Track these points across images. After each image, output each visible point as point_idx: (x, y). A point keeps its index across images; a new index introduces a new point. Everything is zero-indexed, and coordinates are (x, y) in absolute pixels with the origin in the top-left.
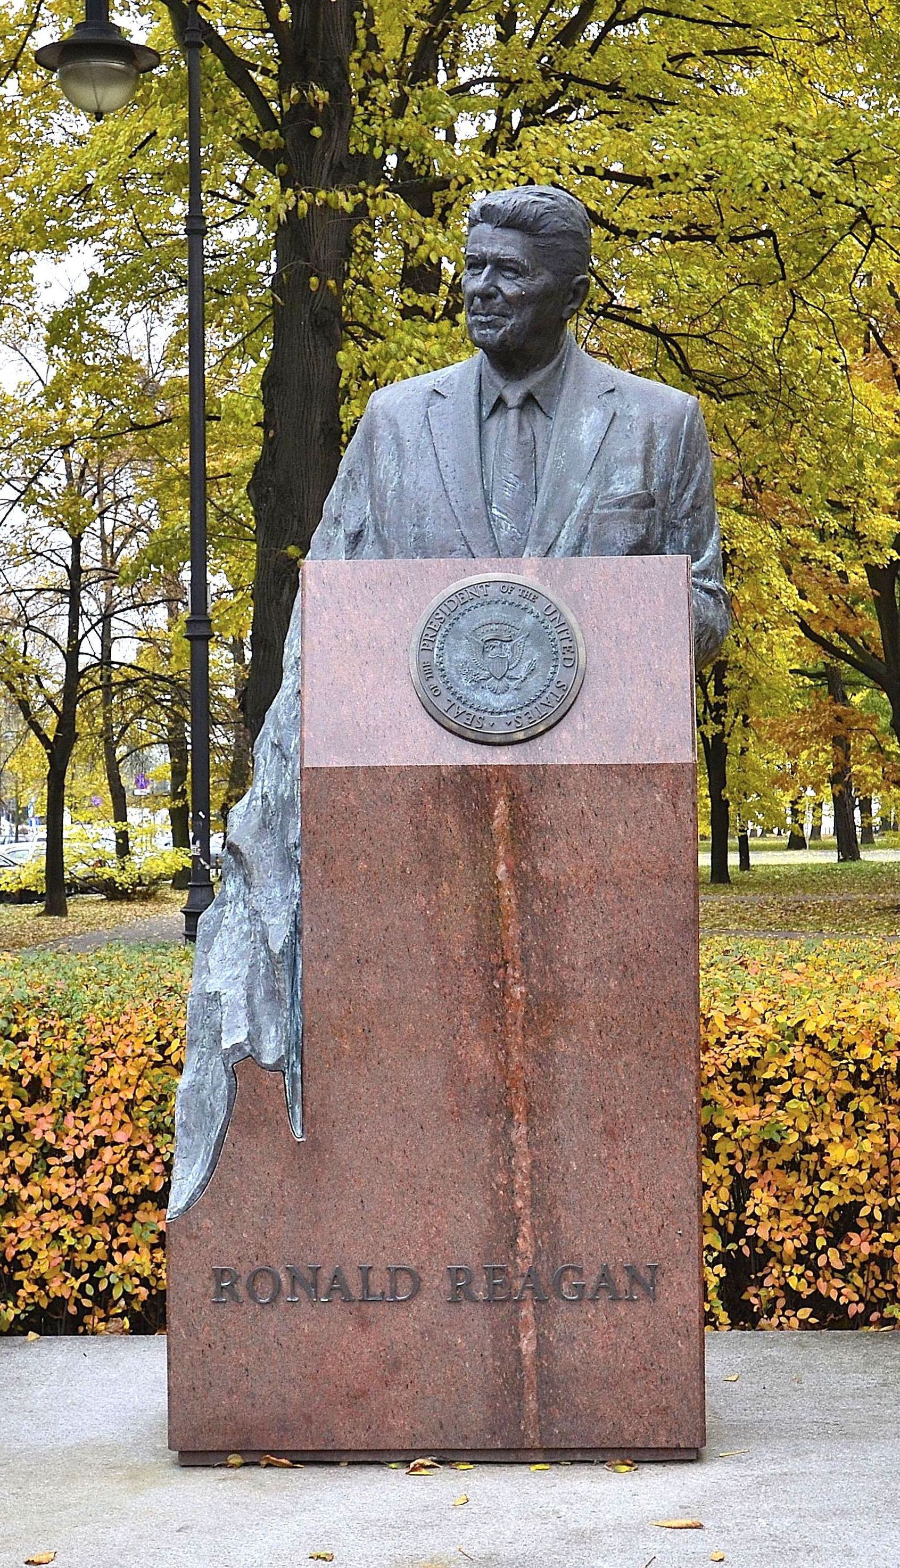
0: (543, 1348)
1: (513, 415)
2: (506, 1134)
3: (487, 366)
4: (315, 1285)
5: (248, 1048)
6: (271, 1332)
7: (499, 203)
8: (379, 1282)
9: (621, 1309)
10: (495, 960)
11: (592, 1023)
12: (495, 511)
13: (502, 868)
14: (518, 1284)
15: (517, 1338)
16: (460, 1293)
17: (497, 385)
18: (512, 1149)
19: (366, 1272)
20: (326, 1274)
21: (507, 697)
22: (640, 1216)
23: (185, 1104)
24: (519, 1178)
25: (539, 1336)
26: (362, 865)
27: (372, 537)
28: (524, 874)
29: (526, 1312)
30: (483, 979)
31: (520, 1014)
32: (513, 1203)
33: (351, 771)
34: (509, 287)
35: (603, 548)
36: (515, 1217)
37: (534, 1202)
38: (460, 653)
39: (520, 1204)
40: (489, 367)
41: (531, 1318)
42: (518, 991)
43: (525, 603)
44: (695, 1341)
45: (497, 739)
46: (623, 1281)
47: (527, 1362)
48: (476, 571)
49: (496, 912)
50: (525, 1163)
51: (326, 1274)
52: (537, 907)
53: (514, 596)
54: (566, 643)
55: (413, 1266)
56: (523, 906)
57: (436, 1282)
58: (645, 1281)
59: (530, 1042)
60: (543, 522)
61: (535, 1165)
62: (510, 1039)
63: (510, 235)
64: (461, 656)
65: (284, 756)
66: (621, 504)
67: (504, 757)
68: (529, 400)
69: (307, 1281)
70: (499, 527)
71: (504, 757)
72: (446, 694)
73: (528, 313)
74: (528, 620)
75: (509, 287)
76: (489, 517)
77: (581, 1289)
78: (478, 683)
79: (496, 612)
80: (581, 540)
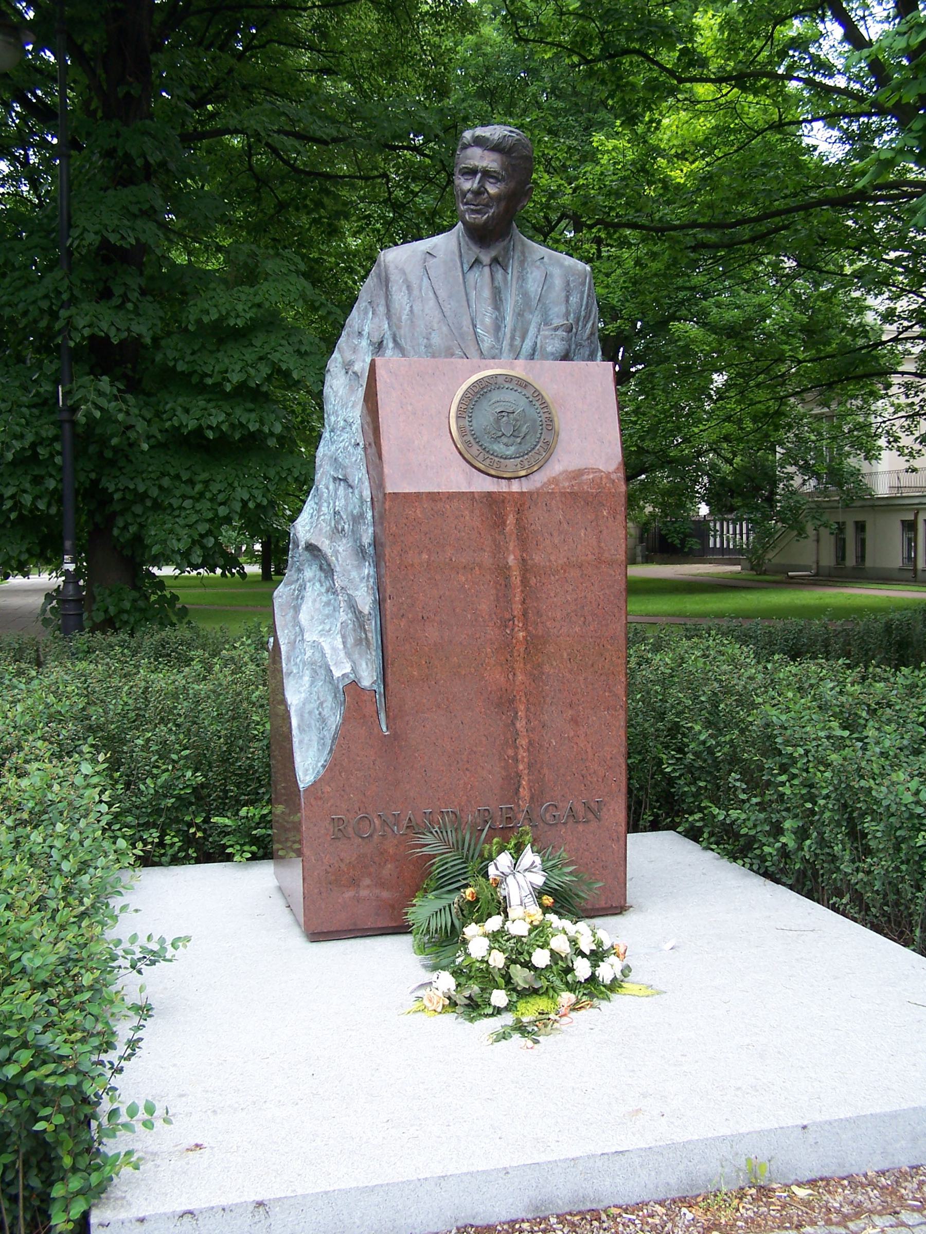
1: (487, 270)
3: (465, 240)
7: (487, 134)
9: (580, 828)
10: (508, 616)
11: (565, 655)
17: (475, 251)
21: (513, 448)
24: (521, 751)
27: (391, 345)
30: (499, 628)
31: (522, 650)
33: (418, 495)
34: (492, 189)
35: (545, 357)
36: (519, 776)
37: (530, 766)
39: (521, 767)
44: (622, 843)
48: (487, 367)
50: (524, 742)
56: (525, 581)
58: (594, 811)
59: (528, 667)
60: (513, 338)
61: (530, 743)
62: (516, 665)
63: (495, 156)
65: (351, 486)
68: (495, 261)
70: (483, 341)
71: (515, 487)
72: (476, 447)
73: (503, 204)
75: (492, 189)
76: (475, 333)
78: (497, 439)
80: (534, 350)
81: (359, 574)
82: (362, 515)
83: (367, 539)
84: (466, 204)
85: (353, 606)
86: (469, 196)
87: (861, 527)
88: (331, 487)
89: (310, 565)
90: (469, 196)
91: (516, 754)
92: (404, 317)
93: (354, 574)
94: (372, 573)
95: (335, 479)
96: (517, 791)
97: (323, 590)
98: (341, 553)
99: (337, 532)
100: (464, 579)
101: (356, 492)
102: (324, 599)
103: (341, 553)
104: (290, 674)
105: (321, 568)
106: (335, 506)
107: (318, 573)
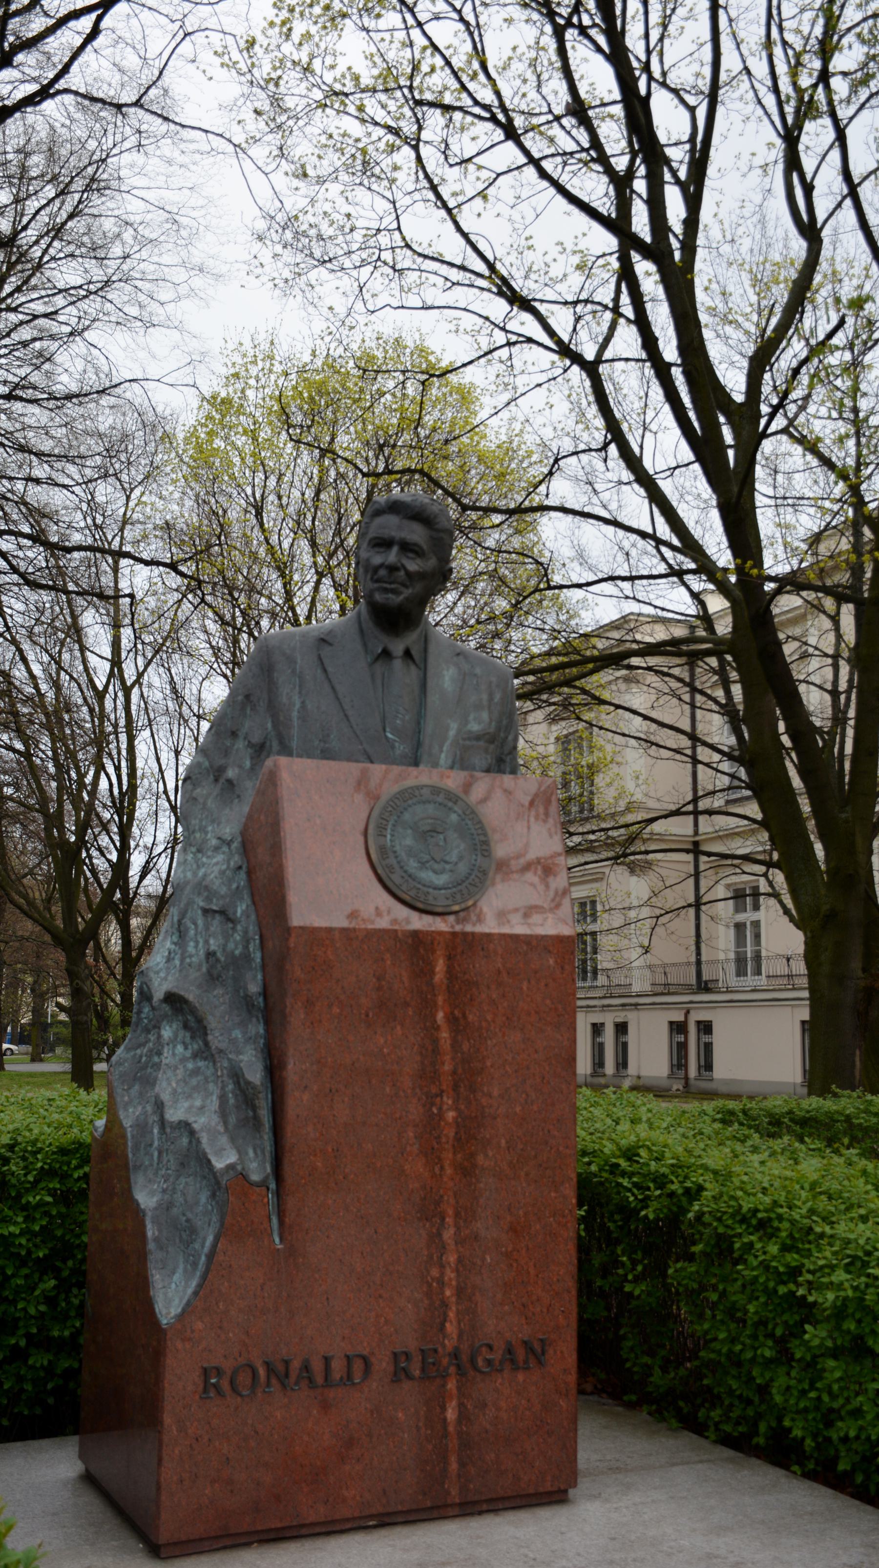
0: (463, 1416)
2: (439, 1235)
4: (287, 1375)
5: (239, 1168)
6: (250, 1422)
8: (338, 1367)
9: (521, 1377)
10: (434, 1090)
11: (503, 1142)
12: (389, 735)
13: (440, 1015)
14: (445, 1361)
15: (443, 1409)
16: (400, 1374)
17: (380, 641)
18: (443, 1248)
19: (327, 1360)
20: (296, 1365)
22: (534, 1298)
23: (155, 1221)
25: (461, 1405)
26: (336, 1010)
28: (456, 1019)
29: (451, 1385)
32: (443, 1293)
36: (445, 1305)
37: (460, 1292)
38: (404, 841)
39: (448, 1293)
40: (371, 624)
41: (455, 1391)
42: (451, 1115)
43: (450, 804)
45: (440, 910)
46: (520, 1354)
47: (451, 1429)
49: (436, 1051)
50: (452, 1258)
51: (296, 1365)
52: (465, 1047)
53: (440, 798)
54: (482, 838)
55: (365, 1353)
56: (455, 1045)
57: (382, 1364)
61: (460, 1260)
64: (409, 842)
65: (229, 920)
66: (478, 738)
67: (440, 925)
69: (279, 1373)
74: (454, 817)
75: (413, 566)
77: (489, 1362)
78: (423, 865)
79: (431, 809)
81: (244, 1033)
82: (247, 957)
83: (254, 988)
84: (377, 581)
85: (236, 1075)
86: (382, 572)
87: (621, 1028)
88: (200, 922)
89: (170, 1022)
90: (382, 572)
91: (442, 1274)
92: (295, 714)
93: (237, 1034)
94: (262, 1031)
95: (206, 912)
96: (442, 1328)
97: (188, 1053)
98: (216, 1007)
99: (213, 978)
100: (382, 1041)
101: (239, 927)
102: (190, 1066)
103: (216, 1007)
104: (137, 1168)
105: (186, 1026)
106: (206, 942)
107: (182, 1033)
